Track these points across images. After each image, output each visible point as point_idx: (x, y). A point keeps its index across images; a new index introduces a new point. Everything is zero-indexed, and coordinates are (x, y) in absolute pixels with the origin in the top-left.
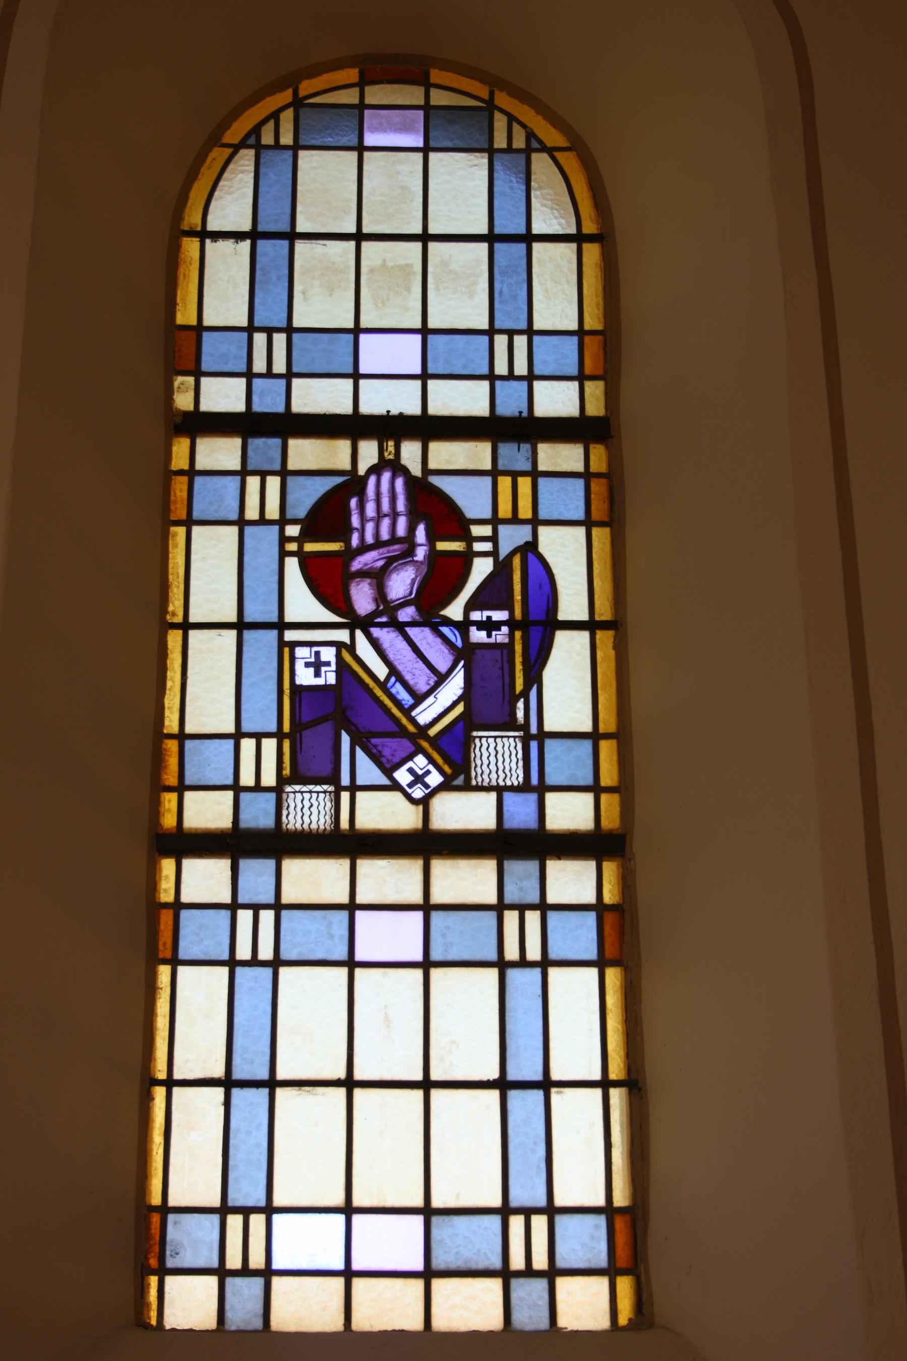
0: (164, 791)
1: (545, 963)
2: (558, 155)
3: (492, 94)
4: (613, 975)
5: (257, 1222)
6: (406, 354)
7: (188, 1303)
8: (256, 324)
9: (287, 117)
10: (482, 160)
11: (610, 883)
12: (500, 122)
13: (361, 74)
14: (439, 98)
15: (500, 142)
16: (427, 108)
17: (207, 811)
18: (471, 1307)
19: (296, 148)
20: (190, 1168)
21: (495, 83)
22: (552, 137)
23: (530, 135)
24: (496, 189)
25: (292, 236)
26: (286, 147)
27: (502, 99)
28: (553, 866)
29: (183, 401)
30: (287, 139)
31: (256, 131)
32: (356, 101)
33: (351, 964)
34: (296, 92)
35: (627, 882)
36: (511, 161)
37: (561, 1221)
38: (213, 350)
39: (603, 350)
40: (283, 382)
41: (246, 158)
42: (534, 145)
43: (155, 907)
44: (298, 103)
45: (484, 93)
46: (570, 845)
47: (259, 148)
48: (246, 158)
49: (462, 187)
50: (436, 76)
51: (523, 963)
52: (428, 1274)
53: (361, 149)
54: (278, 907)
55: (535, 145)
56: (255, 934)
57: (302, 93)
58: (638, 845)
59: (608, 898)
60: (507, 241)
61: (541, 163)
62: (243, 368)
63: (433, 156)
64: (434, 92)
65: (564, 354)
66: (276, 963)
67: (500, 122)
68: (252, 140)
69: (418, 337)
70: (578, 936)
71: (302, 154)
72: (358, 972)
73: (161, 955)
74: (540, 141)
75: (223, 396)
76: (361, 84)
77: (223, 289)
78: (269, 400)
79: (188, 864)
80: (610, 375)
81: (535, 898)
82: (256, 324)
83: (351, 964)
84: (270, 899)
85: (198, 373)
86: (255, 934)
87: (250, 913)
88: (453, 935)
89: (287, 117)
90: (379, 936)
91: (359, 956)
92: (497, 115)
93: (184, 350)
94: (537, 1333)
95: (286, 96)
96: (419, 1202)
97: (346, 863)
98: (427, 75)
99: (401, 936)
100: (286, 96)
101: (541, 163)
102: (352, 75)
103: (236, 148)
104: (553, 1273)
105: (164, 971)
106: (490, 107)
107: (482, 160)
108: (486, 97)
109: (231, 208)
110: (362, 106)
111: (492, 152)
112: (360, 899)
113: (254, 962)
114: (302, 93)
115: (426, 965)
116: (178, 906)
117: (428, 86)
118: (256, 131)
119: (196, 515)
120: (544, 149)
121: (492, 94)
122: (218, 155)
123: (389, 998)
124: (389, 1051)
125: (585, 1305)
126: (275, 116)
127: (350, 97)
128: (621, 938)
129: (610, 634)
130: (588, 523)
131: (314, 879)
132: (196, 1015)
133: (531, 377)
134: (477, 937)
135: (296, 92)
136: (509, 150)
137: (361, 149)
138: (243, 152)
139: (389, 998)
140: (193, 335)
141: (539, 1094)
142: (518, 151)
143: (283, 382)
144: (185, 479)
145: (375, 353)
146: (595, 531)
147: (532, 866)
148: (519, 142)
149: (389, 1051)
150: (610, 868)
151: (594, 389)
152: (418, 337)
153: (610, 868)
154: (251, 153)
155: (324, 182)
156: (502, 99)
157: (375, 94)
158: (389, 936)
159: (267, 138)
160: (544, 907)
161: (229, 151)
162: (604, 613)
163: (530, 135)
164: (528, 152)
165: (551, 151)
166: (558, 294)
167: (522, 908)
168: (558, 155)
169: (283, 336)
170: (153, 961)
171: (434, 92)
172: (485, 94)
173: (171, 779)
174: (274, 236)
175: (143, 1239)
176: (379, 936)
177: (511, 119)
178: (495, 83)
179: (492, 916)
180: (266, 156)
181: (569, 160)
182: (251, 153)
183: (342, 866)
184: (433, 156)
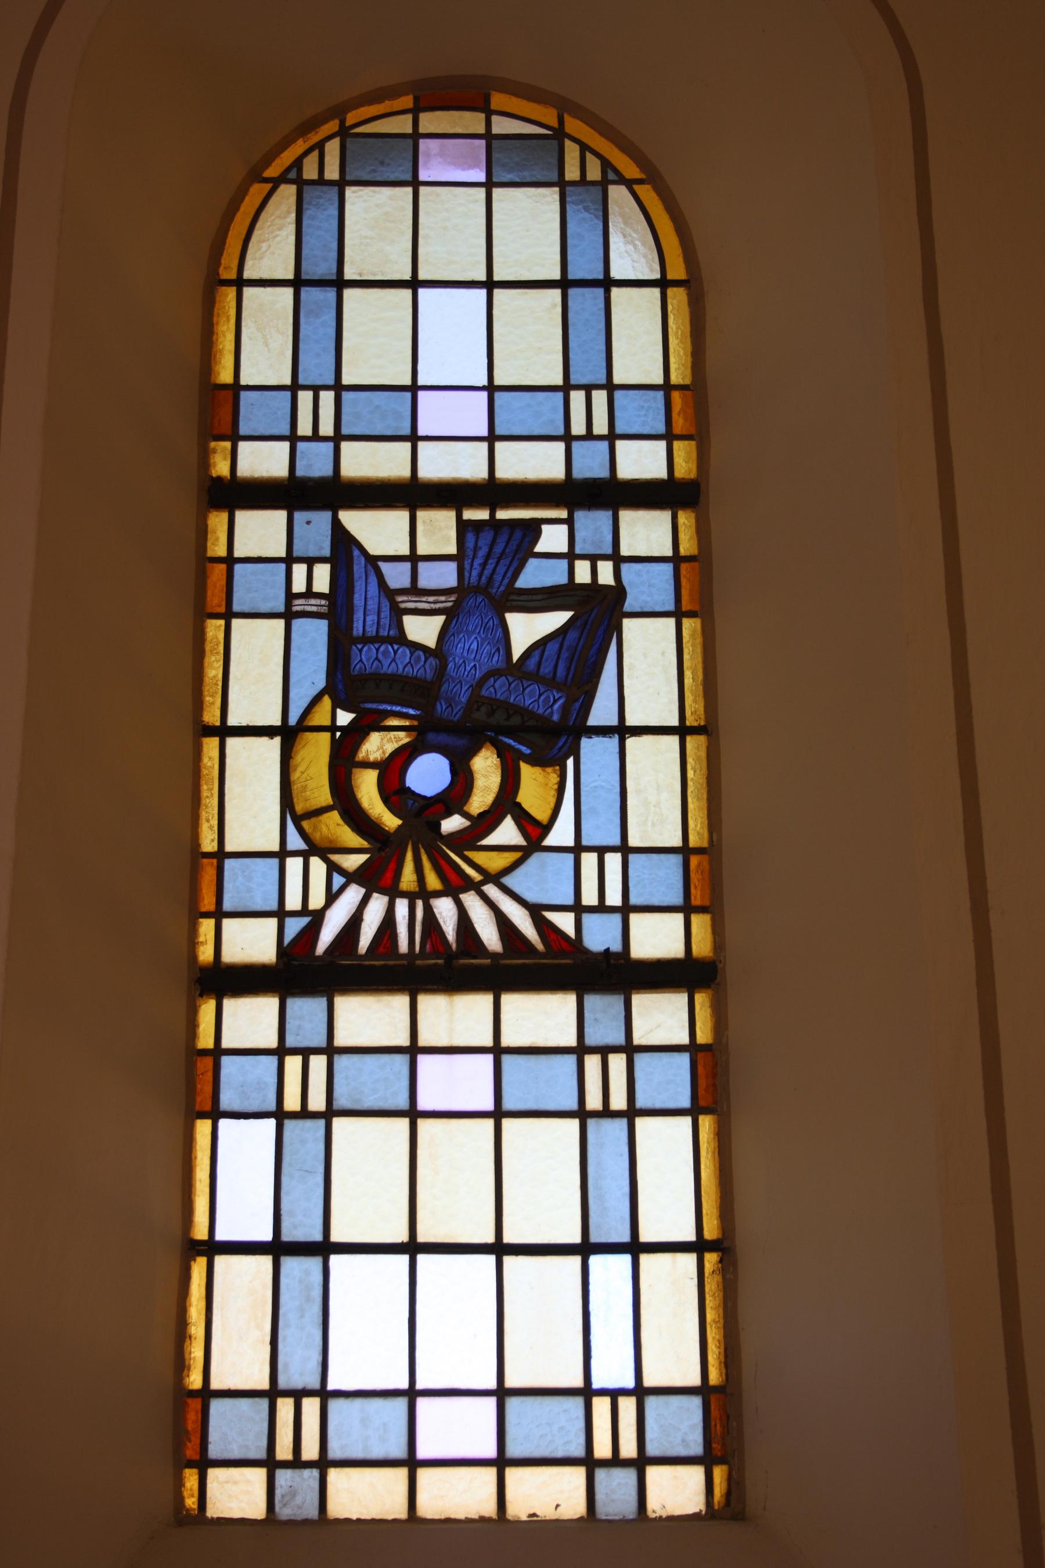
0: (202, 917)
1: (632, 1113)
2: (636, 187)
3: (561, 121)
4: (706, 1123)
5: (318, 1064)
6: (470, 414)
7: (236, 1494)
8: (295, 554)
9: (333, 148)
10: (550, 196)
11: (677, 338)
12: (572, 151)
13: (416, 99)
14: (502, 126)
15: (572, 173)
16: (488, 137)
17: (251, 942)
18: (550, 1495)
19: (341, 184)
20: (235, 1351)
21: (564, 106)
22: (632, 171)
23: (606, 165)
24: (569, 232)
25: (340, 283)
26: (331, 183)
27: (572, 125)
28: (626, 516)
29: (221, 468)
30: (332, 173)
31: (298, 164)
32: (409, 130)
33: (413, 1114)
34: (342, 123)
35: (702, 532)
36: (583, 198)
37: (641, 1060)
38: (253, 413)
39: (690, 406)
40: (330, 445)
41: (287, 193)
42: (611, 175)
43: (205, 561)
44: (344, 133)
45: (550, 117)
46: (660, 975)
47: (301, 184)
48: (287, 193)
49: (530, 225)
50: (498, 100)
51: (606, 1112)
52: (501, 1462)
53: (415, 184)
54: (331, 1050)
55: (611, 176)
56: (306, 1083)
57: (349, 122)
58: (732, 972)
59: (694, 841)
60: (582, 285)
61: (618, 194)
62: (286, 430)
63: (497, 192)
64: (495, 119)
65: (648, 412)
66: (330, 1113)
67: (572, 151)
68: (293, 175)
69: (489, 1059)
70: (669, 1080)
71: (350, 192)
72: (421, 382)
73: (204, 909)
74: (616, 171)
75: (263, 460)
76: (415, 112)
77: (261, 346)
78: (315, 463)
79: (242, 517)
80: (700, 435)
81: (620, 1039)
82: (295, 554)
83: (413, 1114)
84: (321, 1041)
85: (235, 438)
86: (306, 1083)
87: (310, 394)
88: (525, 1082)
89: (333, 148)
90: (444, 1083)
91: (423, 1452)
92: (568, 143)
93: (220, 410)
94: (624, 1521)
95: (333, 126)
96: (490, 1123)
97: (404, 515)
98: (487, 100)
99: (466, 1083)
100: (333, 126)
101: (618, 194)
102: (407, 102)
103: (276, 183)
104: (642, 1462)
105: (214, 628)
106: (559, 135)
107: (550, 196)
108: (556, 125)
109: (272, 252)
110: (416, 136)
111: (562, 184)
112: (423, 1041)
113: (306, 1053)
114: (349, 122)
115: (498, 1114)
116: (218, 1052)
117: (489, 113)
118: (298, 164)
119: (228, 905)
120: (622, 180)
121: (561, 121)
122: (257, 191)
123: (456, 1154)
124: (457, 1208)
125: (677, 1492)
126: (320, 147)
127: (402, 125)
128: (714, 1086)
129: (702, 739)
130: (678, 614)
131: (369, 1018)
132: (241, 1177)
133: (612, 437)
134: (556, 1082)
135: (342, 123)
136: (583, 181)
137: (415, 184)
138: (283, 187)
139: (456, 1154)
140: (229, 394)
141: (600, 292)
142: (593, 183)
143: (330, 445)
144: (223, 567)
145: (434, 414)
146: (695, 919)
147: (615, 1002)
148: (594, 173)
149: (457, 1208)
150: (686, 519)
151: (700, 923)
152: (489, 1059)
153: (701, 999)
154: (293, 189)
155: (373, 220)
156: (572, 125)
157: (429, 122)
158: (455, 1083)
159: (310, 172)
160: (630, 1049)
161: (268, 186)
162: (711, 1233)
163: (606, 165)
164: (604, 184)
165: (629, 184)
166: (641, 342)
167: (616, 1461)
168: (636, 187)
169: (331, 395)
170: (202, 614)
171: (495, 119)
172: (554, 122)
173: (208, 903)
174: (317, 281)
175: (183, 1416)
176: (444, 1083)
177: (584, 148)
178: (564, 106)
179: (571, 1060)
180: (309, 192)
181: (645, 192)
182: (293, 189)
183: (401, 517)
184: (497, 192)
